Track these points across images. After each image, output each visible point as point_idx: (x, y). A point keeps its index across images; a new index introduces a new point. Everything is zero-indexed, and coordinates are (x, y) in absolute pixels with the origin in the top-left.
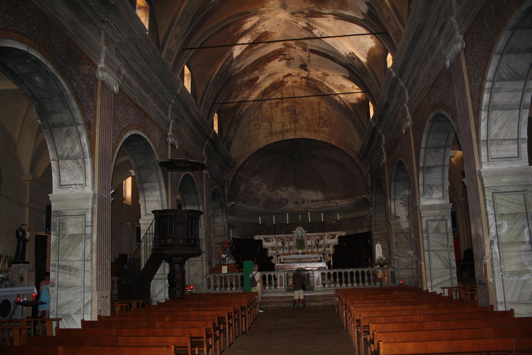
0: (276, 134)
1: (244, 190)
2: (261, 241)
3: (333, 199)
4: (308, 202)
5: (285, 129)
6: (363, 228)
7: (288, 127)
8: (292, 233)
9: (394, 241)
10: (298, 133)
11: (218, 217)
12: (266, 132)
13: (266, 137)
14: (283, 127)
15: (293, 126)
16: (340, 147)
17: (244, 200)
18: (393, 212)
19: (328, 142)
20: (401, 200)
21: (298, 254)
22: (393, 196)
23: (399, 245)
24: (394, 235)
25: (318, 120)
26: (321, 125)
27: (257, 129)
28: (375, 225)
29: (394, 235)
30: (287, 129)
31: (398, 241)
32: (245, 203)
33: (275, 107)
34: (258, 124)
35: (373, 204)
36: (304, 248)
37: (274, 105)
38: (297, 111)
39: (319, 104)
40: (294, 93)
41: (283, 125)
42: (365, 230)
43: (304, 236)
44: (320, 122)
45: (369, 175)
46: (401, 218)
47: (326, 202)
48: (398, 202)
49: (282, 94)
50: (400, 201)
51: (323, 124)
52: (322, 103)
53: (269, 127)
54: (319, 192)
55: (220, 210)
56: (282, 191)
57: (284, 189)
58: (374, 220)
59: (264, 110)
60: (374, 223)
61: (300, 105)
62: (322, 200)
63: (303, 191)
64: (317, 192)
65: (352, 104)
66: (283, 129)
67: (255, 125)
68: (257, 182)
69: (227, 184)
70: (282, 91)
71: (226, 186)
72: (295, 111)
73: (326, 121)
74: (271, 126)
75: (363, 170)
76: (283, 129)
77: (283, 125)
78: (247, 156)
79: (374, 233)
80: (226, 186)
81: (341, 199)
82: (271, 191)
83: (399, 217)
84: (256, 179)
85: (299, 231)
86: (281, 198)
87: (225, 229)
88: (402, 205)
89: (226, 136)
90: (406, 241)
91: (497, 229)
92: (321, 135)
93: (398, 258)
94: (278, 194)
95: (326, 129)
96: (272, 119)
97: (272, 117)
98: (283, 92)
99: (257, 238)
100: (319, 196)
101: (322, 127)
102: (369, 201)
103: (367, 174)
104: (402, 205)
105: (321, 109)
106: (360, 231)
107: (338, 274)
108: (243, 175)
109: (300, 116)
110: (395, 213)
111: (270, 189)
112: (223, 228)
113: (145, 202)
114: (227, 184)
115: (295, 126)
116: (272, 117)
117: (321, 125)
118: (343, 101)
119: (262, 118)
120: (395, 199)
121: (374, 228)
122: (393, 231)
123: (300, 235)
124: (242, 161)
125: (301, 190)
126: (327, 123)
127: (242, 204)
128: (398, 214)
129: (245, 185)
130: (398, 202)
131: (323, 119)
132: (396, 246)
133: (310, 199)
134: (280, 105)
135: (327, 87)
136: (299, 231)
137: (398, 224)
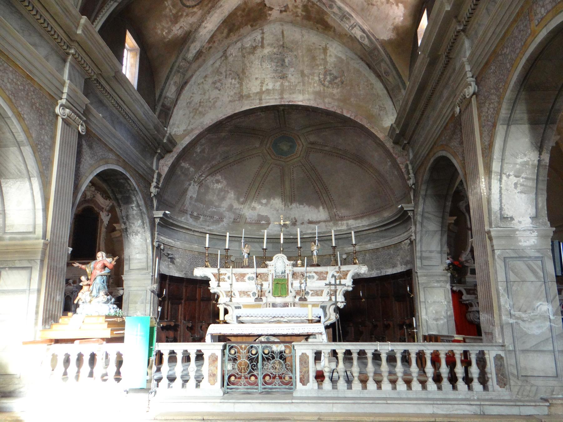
0: (248, 96)
1: (195, 196)
2: (205, 282)
3: (342, 219)
4: (303, 223)
5: (264, 89)
6: (394, 266)
7: (270, 87)
8: (266, 266)
9: (501, 276)
10: (286, 96)
11: (136, 234)
12: (232, 93)
13: (230, 101)
14: (262, 86)
15: (279, 83)
16: (358, 121)
17: (195, 214)
18: (495, 206)
19: (339, 111)
20: (516, 176)
21: (274, 305)
22: (496, 166)
23: (514, 288)
24: (500, 265)
25: (321, 76)
26: (327, 83)
27: (217, 88)
28: (421, 258)
29: (500, 265)
30: (267, 90)
31: (512, 277)
32: (197, 218)
33: (250, 53)
34: (220, 80)
35: (419, 218)
36: (287, 293)
37: (248, 50)
38: (286, 60)
39: (325, 50)
40: (283, 32)
41: (262, 83)
42: (400, 269)
43: (287, 272)
44: (325, 79)
45: (410, 167)
46: (515, 221)
47: (331, 223)
48: (510, 181)
49: (263, 33)
50: (515, 180)
51: (330, 82)
52: (330, 49)
53: (237, 86)
54: (321, 208)
55: (140, 222)
56: (262, 204)
57: (264, 201)
58: (418, 248)
59: (231, 59)
60: (418, 254)
61: (291, 51)
62: (325, 221)
63: (294, 205)
64: (317, 207)
65: (383, 43)
66: (261, 89)
67: (214, 83)
68: (219, 186)
69: (155, 176)
70: (262, 30)
71: (155, 180)
72: (284, 61)
73: (336, 78)
74: (241, 84)
75: (399, 160)
76: (261, 89)
77: (262, 83)
78: (197, 132)
79: (420, 272)
80: (155, 180)
81: (356, 218)
82: (242, 203)
83: (512, 219)
84: (218, 182)
85: (280, 264)
86: (259, 215)
87: (147, 258)
88: (519, 189)
89: (160, 96)
90: (533, 278)
91: (266, 335)
92: (326, 100)
93: (511, 321)
94: (254, 209)
95: (335, 91)
96: (243, 72)
97: (243, 70)
98: (265, 31)
99: (199, 272)
100: (321, 214)
101: (328, 87)
102: (410, 214)
103: (407, 166)
104: (519, 189)
105: (328, 59)
106: (390, 271)
107: (355, 356)
108: (192, 169)
109: (292, 69)
110: (501, 209)
111: (242, 200)
112: (145, 256)
113: (219, 281)
114: (155, 176)
115: (282, 85)
116: (243, 70)
117: (327, 83)
118: (368, 37)
119: (226, 71)
120: (501, 174)
121: (418, 263)
122: (497, 252)
123: (280, 269)
124: (187, 141)
125: (291, 203)
126: (336, 81)
127: (191, 221)
128: (508, 212)
129: (197, 188)
130: (510, 181)
131: (330, 74)
132: (508, 290)
133: (306, 219)
134: (259, 50)
135: (340, 8)
136: (280, 264)
137: (510, 235)
